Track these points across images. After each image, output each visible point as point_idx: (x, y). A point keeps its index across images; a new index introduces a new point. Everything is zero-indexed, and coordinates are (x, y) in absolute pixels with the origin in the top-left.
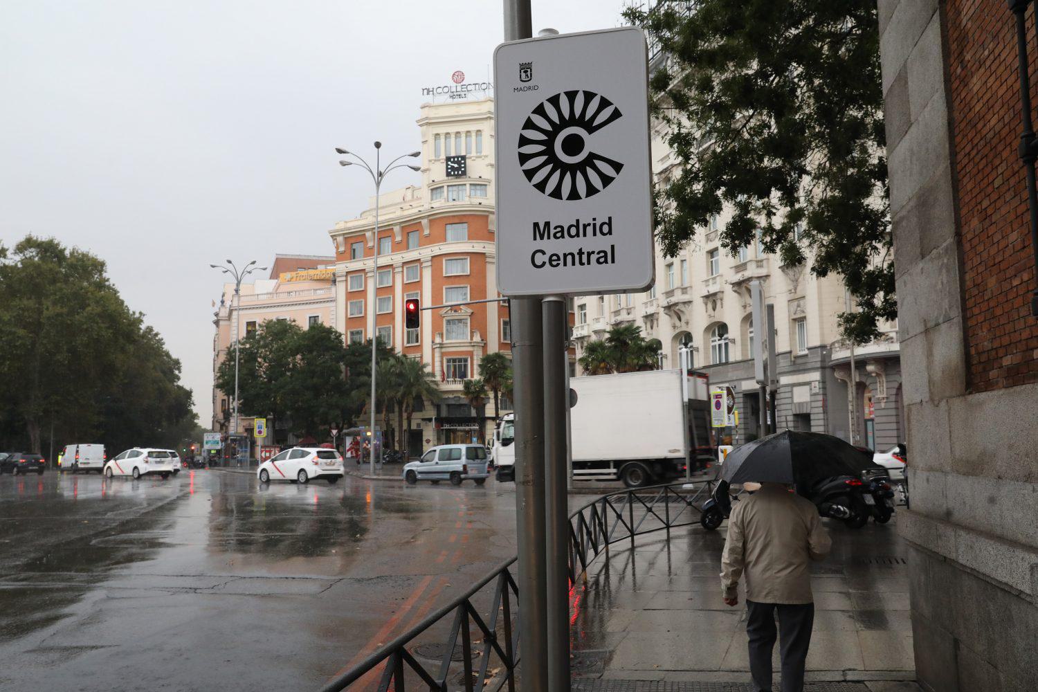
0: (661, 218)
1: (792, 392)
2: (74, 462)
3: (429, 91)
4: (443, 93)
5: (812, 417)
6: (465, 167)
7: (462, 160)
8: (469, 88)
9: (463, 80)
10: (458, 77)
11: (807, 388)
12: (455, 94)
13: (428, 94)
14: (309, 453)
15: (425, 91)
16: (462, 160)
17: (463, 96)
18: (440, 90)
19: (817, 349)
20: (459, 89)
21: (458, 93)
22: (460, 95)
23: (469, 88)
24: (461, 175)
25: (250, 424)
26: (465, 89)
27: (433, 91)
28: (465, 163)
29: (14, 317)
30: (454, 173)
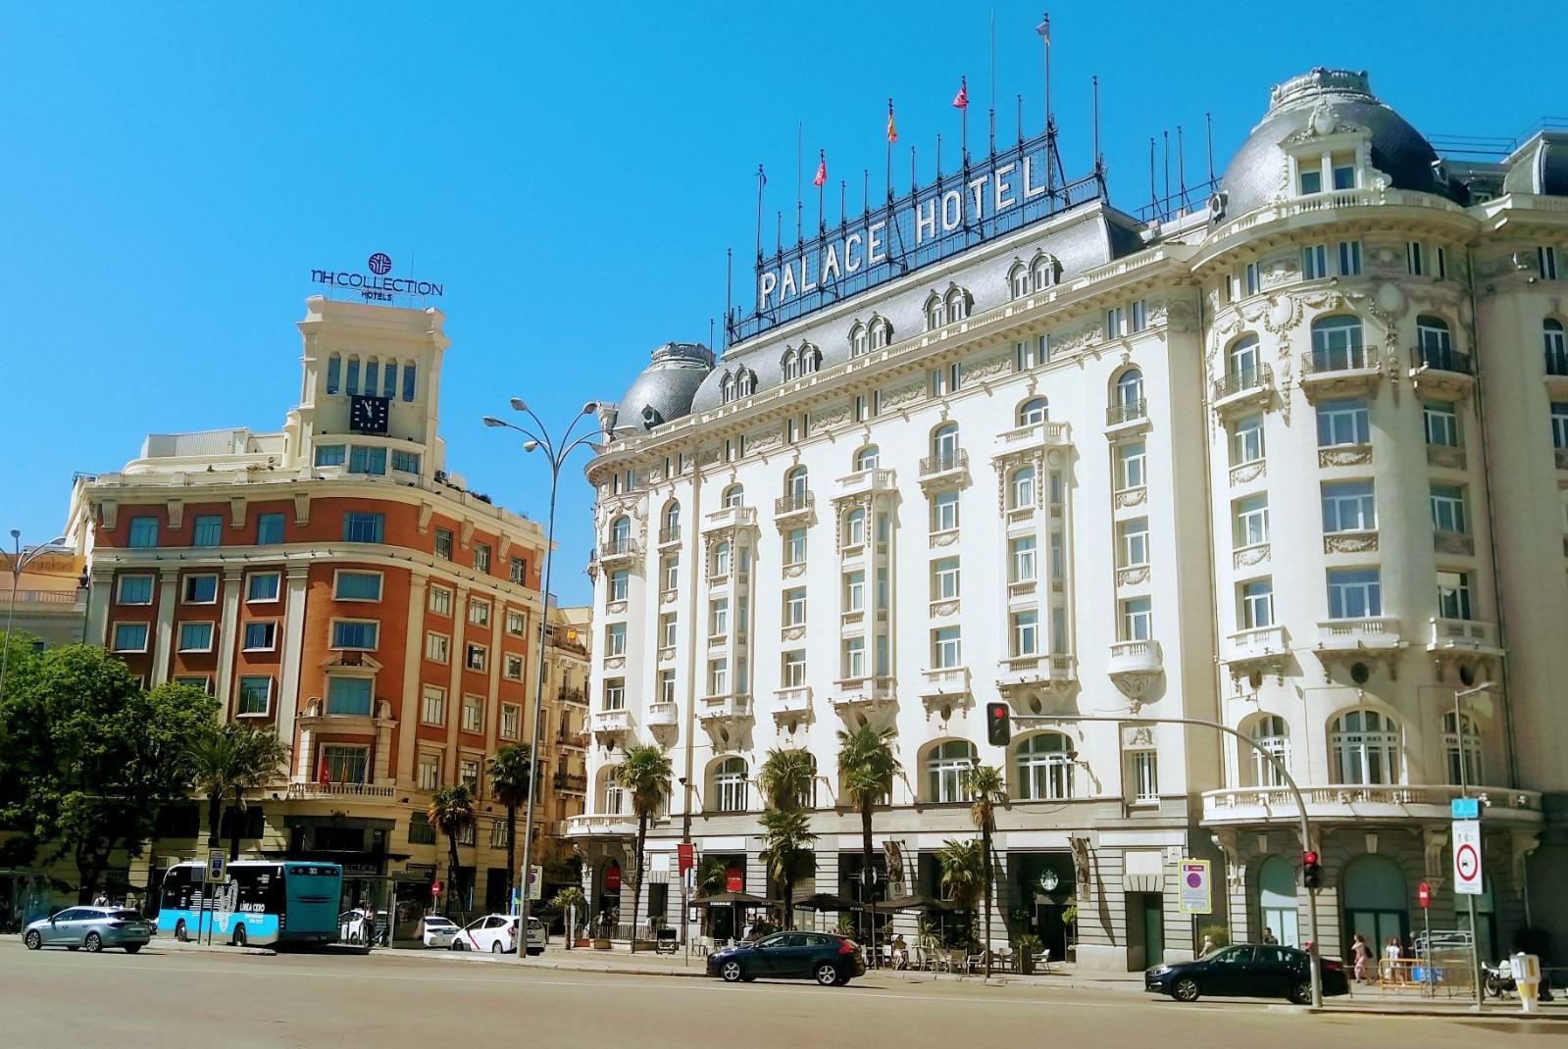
0: (104, 681)
1: (1123, 857)
2: (931, 715)
3: (324, 277)
4: (349, 286)
5: (1165, 898)
6: (386, 418)
7: (359, 423)
8: (398, 285)
9: (387, 270)
10: (380, 263)
11: (1158, 854)
12: (373, 290)
13: (322, 281)
14: (505, 922)
15: (318, 276)
16: (359, 423)
17: (387, 297)
18: (344, 279)
19: (1180, 801)
20: (379, 283)
21: (378, 291)
22: (380, 295)
23: (398, 285)
24: (378, 430)
25: (1138, 708)
26: (391, 287)
27: (332, 278)
28: (386, 412)
29: (163, 743)
30: (382, 418)
